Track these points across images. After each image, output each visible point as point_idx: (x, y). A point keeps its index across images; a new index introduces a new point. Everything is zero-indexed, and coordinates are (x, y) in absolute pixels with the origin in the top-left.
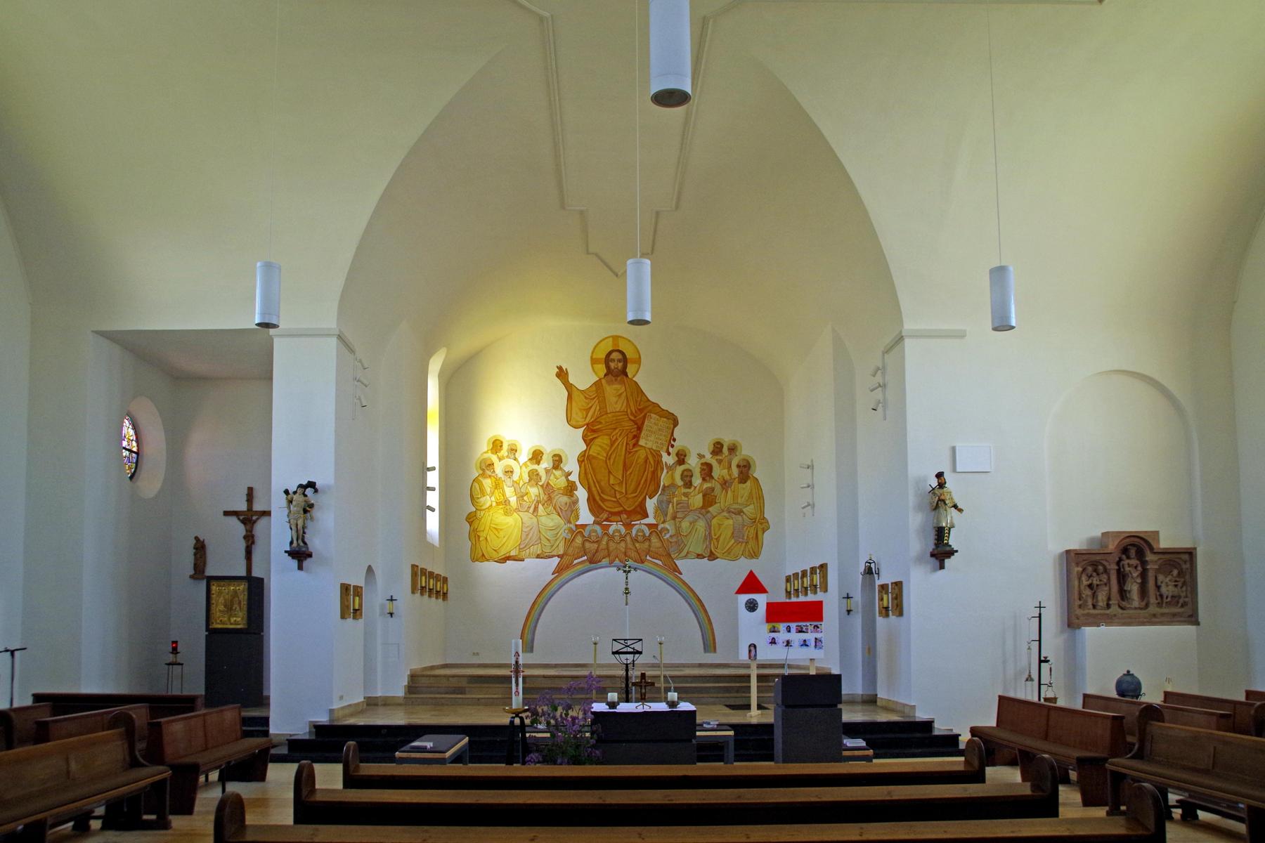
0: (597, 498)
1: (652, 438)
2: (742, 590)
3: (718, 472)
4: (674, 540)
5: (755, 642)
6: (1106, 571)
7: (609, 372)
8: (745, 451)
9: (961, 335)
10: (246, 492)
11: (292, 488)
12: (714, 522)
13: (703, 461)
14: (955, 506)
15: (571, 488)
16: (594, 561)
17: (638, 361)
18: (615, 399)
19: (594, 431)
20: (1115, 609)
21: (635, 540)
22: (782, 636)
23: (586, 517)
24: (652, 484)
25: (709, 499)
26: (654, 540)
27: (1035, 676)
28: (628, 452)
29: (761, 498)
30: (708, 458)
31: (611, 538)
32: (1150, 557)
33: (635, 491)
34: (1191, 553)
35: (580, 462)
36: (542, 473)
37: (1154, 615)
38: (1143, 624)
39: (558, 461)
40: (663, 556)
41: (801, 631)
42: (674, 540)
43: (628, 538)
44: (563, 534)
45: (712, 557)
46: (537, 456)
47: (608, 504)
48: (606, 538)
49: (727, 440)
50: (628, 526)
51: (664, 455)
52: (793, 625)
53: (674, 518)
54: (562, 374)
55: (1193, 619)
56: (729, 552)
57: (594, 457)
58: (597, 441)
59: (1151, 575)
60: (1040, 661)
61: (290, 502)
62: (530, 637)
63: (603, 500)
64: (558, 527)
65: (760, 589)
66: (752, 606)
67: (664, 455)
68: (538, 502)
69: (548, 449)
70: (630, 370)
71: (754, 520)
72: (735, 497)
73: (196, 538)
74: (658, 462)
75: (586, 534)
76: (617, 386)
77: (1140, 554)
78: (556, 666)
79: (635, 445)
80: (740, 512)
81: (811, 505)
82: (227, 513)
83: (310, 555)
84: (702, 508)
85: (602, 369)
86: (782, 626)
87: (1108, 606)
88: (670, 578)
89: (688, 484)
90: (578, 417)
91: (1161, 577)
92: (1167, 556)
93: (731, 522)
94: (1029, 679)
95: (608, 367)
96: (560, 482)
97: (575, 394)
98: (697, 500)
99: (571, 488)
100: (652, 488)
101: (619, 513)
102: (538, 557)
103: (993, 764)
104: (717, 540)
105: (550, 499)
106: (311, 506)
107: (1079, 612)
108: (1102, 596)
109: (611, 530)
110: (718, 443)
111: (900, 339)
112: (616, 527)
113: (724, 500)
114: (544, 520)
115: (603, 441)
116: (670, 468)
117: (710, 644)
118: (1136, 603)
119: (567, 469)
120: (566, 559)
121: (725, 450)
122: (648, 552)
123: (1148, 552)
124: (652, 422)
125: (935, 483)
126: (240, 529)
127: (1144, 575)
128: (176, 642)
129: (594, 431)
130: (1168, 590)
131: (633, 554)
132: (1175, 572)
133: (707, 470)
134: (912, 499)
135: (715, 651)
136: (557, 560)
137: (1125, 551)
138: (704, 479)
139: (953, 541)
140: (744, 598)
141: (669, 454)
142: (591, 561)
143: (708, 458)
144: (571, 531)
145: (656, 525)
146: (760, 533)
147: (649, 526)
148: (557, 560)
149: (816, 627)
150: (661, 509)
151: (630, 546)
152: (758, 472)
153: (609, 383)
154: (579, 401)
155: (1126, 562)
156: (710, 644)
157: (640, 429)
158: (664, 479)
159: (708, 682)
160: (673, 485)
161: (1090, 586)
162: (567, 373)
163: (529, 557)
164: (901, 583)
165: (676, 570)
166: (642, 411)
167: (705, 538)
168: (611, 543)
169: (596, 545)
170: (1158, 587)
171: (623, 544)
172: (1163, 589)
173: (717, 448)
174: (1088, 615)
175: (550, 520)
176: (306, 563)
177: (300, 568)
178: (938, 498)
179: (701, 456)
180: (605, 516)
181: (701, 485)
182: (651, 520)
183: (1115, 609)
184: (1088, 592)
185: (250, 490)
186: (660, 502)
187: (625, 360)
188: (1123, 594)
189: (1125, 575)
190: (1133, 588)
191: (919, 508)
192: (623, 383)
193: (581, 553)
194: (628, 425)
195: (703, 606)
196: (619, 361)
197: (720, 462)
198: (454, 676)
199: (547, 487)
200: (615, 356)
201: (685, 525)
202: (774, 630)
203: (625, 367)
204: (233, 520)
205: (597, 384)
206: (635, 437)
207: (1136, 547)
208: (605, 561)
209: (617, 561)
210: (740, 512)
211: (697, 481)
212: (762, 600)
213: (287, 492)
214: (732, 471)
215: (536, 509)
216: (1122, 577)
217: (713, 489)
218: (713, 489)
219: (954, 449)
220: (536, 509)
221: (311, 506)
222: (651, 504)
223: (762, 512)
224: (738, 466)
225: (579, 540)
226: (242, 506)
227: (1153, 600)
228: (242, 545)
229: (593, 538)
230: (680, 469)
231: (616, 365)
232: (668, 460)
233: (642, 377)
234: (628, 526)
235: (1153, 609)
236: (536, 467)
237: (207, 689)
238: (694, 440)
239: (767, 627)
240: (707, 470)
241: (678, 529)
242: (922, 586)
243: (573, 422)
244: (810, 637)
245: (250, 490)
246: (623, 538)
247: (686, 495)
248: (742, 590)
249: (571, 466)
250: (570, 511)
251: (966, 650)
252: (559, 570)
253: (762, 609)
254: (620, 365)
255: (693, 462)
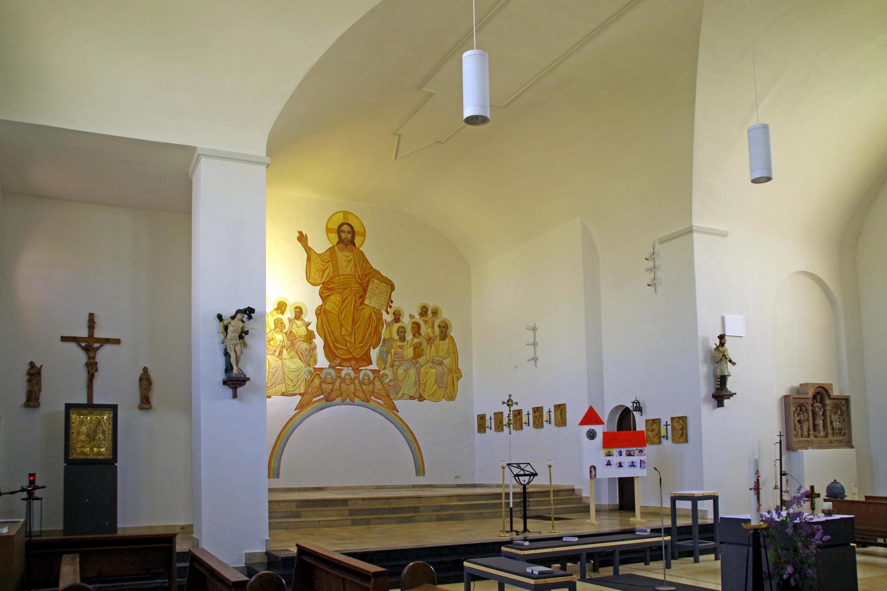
0: (332, 346)
1: (375, 299)
2: (583, 423)
3: (424, 330)
4: (392, 383)
5: (490, 464)
6: (806, 410)
7: (341, 241)
8: (445, 315)
9: (724, 235)
10: (86, 318)
11: (227, 313)
12: (422, 370)
13: (413, 320)
14: (730, 361)
15: (310, 337)
16: (329, 400)
17: (363, 234)
18: (345, 264)
19: (328, 289)
20: (812, 438)
21: (362, 383)
22: (615, 459)
23: (322, 362)
24: (374, 338)
25: (418, 351)
26: (377, 383)
27: (778, 484)
28: (356, 309)
29: (456, 352)
30: (417, 318)
31: (343, 380)
32: (828, 402)
33: (361, 342)
34: (847, 400)
35: (318, 314)
36: (286, 322)
37: (831, 442)
38: (827, 447)
39: (299, 312)
40: (381, 396)
41: (629, 455)
42: (392, 383)
43: (356, 381)
44: (304, 375)
45: (421, 398)
46: (281, 307)
47: (340, 352)
48: (339, 381)
49: (431, 305)
50: (357, 371)
51: (384, 313)
52: (624, 450)
53: (392, 366)
54: (302, 238)
55: (849, 444)
56: (433, 395)
57: (329, 311)
58: (332, 298)
59: (828, 413)
60: (781, 475)
61: (226, 328)
62: (276, 465)
63: (335, 347)
64: (298, 370)
65: (599, 422)
66: (592, 435)
67: (384, 313)
68: (283, 347)
69: (292, 301)
70: (358, 240)
71: (451, 371)
72: (437, 352)
73: (32, 364)
74: (380, 318)
75: (323, 376)
76: (347, 253)
77: (822, 401)
78: (299, 490)
79: (362, 303)
80: (441, 363)
81: (535, 359)
82: (64, 339)
83: (249, 379)
84: (413, 358)
85: (335, 238)
86: (615, 451)
87: (809, 435)
88: (390, 414)
89: (403, 339)
90: (315, 275)
91: (833, 416)
92: (835, 401)
93: (434, 371)
94: (775, 488)
95: (340, 237)
96: (301, 331)
97: (313, 257)
98: (409, 352)
99: (310, 337)
100: (375, 340)
101: (349, 360)
102: (283, 394)
103: (80, 556)
104: (425, 385)
105: (293, 344)
106: (247, 333)
107: (795, 439)
108: (805, 429)
109: (343, 374)
110: (424, 307)
111: (690, 231)
112: (346, 371)
113: (430, 352)
114: (288, 363)
115: (335, 298)
116: (388, 325)
117: (420, 470)
118: (822, 434)
119: (306, 320)
120: (307, 396)
121: (429, 312)
122: (373, 393)
123: (826, 398)
124: (374, 285)
125: (718, 342)
126: (81, 357)
127: (824, 414)
128: (33, 475)
129: (328, 289)
130: (837, 424)
131: (361, 395)
132: (839, 412)
133: (416, 328)
134: (701, 355)
135: (424, 475)
136: (298, 398)
137: (814, 397)
138: (414, 335)
139: (730, 386)
140: (587, 428)
141: (388, 313)
142: (327, 399)
143: (417, 318)
144: (310, 373)
145: (379, 371)
146: (455, 381)
147: (373, 371)
148: (298, 398)
149: (641, 451)
150: (382, 358)
151: (358, 387)
152: (453, 332)
153: (341, 250)
154: (316, 264)
155: (816, 404)
156: (420, 470)
157: (365, 290)
158: (384, 333)
159: (490, 499)
160: (391, 339)
161: (799, 421)
162: (306, 238)
163: (275, 394)
164: (683, 419)
165: (394, 408)
166: (366, 277)
167: (416, 383)
168: (343, 385)
169: (330, 386)
170: (831, 422)
171: (352, 386)
172: (834, 424)
173: (424, 311)
174: (800, 441)
175: (293, 364)
176: (240, 390)
177: (235, 396)
178: (719, 355)
179: (412, 317)
180: (338, 361)
181: (412, 340)
182: (374, 366)
183: (812, 438)
184: (798, 425)
185: (91, 317)
186: (381, 352)
187: (353, 232)
188: (815, 426)
189: (815, 413)
190: (820, 422)
191: (705, 361)
192: (351, 251)
193: (320, 392)
194: (356, 286)
195: (415, 438)
196: (349, 232)
197: (426, 322)
198: (284, 501)
199: (290, 335)
200: (345, 228)
201: (401, 371)
202: (609, 454)
203: (353, 237)
204: (73, 346)
205: (331, 250)
206: (361, 297)
207: (821, 393)
208: (339, 400)
209: (348, 400)
210: (441, 363)
211: (409, 336)
212: (599, 430)
213: (220, 317)
214: (434, 332)
215: (281, 353)
216: (814, 414)
217: (420, 344)
218: (420, 344)
219: (723, 319)
220: (281, 353)
221: (247, 333)
222: (374, 353)
223: (457, 364)
224: (439, 327)
225: (317, 381)
226: (84, 333)
227: (830, 431)
228: (83, 375)
229: (329, 380)
230: (396, 326)
231: (346, 236)
232: (388, 318)
233: (368, 247)
234: (357, 371)
235: (830, 437)
236: (280, 316)
237: (65, 524)
238: (407, 303)
239: (603, 452)
240: (416, 328)
241: (395, 375)
242: (709, 421)
243: (311, 280)
244: (636, 459)
245: (91, 317)
246: (352, 381)
247: (401, 347)
248: (583, 423)
249: (310, 317)
250: (309, 356)
251: (736, 465)
252: (300, 407)
253: (599, 437)
254: (349, 236)
255: (406, 321)
